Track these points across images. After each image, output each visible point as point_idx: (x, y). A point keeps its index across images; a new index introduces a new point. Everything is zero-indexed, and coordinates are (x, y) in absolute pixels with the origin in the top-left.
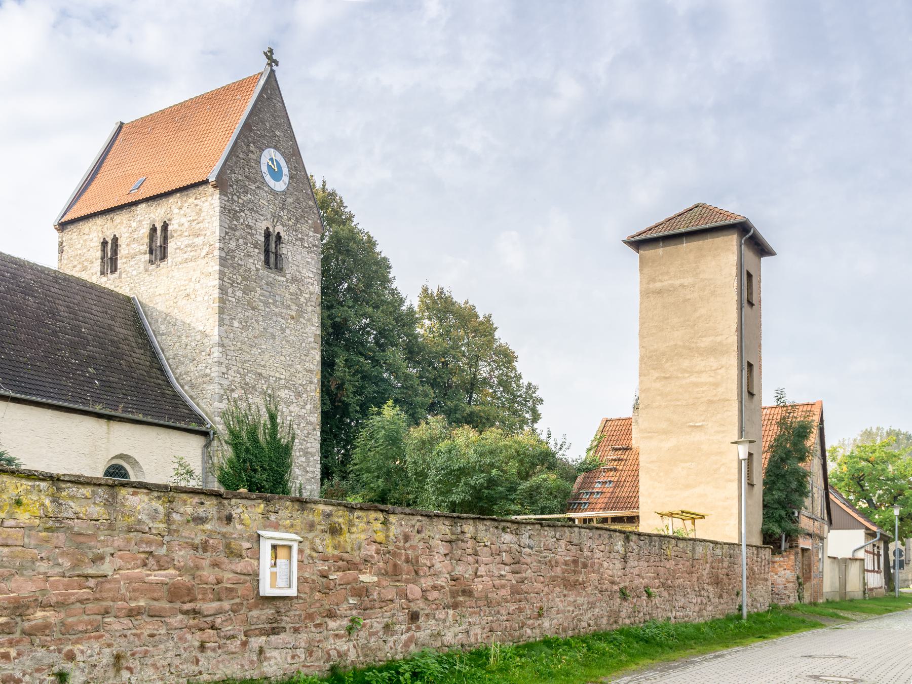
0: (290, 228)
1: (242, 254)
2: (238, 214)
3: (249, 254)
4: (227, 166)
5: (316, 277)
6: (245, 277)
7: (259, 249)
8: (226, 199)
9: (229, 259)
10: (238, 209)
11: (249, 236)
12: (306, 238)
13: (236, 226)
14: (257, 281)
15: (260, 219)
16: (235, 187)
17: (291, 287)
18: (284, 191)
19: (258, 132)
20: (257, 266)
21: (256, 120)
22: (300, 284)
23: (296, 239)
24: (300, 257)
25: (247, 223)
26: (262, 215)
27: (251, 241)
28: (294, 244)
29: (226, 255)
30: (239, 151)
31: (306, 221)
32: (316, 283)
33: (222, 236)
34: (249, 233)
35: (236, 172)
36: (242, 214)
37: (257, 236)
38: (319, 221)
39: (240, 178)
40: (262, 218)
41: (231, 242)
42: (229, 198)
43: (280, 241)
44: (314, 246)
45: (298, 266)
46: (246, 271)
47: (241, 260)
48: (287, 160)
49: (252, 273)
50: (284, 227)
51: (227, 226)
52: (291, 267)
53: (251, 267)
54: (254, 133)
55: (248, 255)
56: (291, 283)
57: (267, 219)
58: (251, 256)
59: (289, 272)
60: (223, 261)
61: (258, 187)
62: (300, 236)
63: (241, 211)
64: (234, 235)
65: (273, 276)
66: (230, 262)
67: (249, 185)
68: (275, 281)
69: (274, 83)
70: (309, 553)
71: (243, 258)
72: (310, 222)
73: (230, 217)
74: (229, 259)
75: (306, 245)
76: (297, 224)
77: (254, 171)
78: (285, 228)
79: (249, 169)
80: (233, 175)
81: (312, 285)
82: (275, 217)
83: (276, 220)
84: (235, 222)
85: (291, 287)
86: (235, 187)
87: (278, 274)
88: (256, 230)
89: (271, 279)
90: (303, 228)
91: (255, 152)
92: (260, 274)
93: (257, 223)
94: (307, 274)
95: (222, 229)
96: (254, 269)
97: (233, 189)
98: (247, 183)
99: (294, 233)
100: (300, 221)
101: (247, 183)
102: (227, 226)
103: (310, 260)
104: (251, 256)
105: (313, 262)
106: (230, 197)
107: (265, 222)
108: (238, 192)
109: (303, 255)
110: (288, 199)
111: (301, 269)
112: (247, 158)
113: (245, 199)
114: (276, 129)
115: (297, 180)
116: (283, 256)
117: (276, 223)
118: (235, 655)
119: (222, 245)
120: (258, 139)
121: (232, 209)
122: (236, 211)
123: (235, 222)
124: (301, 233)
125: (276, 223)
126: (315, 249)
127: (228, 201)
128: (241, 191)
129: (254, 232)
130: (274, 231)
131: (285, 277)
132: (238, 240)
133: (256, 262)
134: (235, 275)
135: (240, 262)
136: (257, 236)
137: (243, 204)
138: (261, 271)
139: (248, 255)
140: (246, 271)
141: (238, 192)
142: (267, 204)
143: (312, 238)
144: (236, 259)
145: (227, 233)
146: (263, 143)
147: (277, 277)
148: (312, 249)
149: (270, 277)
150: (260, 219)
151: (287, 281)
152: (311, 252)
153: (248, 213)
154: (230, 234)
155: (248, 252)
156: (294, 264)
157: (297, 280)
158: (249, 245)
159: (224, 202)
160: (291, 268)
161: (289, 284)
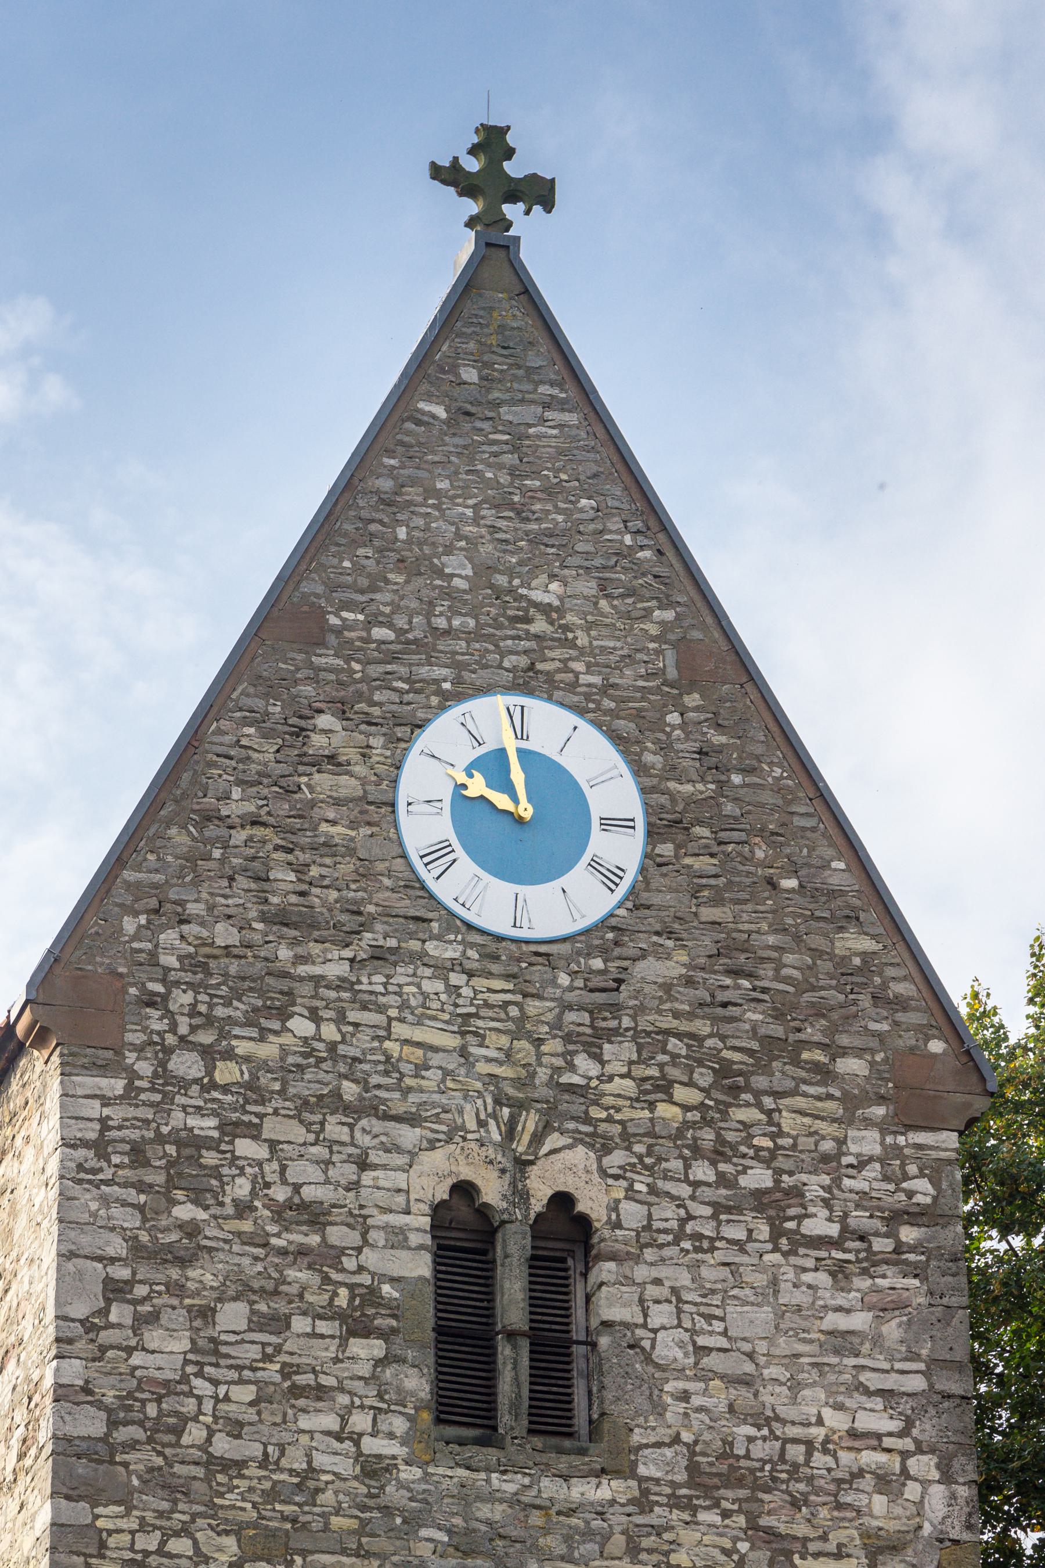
0: (664, 1147)
1: (245, 1394)
2: (210, 1158)
3: (301, 1379)
4: (120, 895)
5: (925, 1429)
6: (273, 1534)
7: (385, 1335)
8: (117, 1086)
9: (132, 1445)
10: (206, 1126)
11: (299, 1275)
12: (815, 1184)
13: (192, 1230)
14: (380, 1544)
15: (393, 1148)
16: (183, 998)
17: (688, 1536)
18: (604, 924)
19: (379, 633)
20: (371, 1445)
21: (358, 568)
22: (773, 1499)
23: (718, 1208)
24: (765, 1314)
25: (280, 1194)
26: (412, 1120)
27: (317, 1299)
28: (704, 1244)
29: (113, 1424)
30: (220, 778)
31: (816, 1067)
32: (923, 1465)
33: (80, 1310)
34: (303, 1251)
35: (193, 908)
36: (245, 1147)
37: (370, 1258)
38: (936, 1046)
39: (225, 934)
40: (409, 1136)
41: (153, 1337)
42: (133, 1075)
43: (588, 1247)
44: (896, 1218)
45: (745, 1381)
46: (273, 1495)
47: (236, 1429)
48: (625, 726)
49: (327, 1497)
50: (606, 1150)
51: (117, 1247)
52: (685, 1396)
53: (321, 1460)
54: (347, 650)
55: (297, 1391)
56: (675, 1502)
57: (455, 1132)
58: (320, 1392)
59: (664, 1434)
60: (82, 1467)
61: (379, 956)
62: (758, 1178)
63: (231, 1130)
64: (176, 1289)
65: (509, 1485)
66: (141, 1459)
67: (301, 959)
68: (536, 1519)
69: (515, 316)
70: (291, 954)
71: (251, 1415)
72: (852, 1066)
73: (141, 1187)
74: (132, 1445)
75: (819, 1225)
76: (724, 1111)
77: (347, 867)
78: (617, 1159)
79: (301, 869)
80: (169, 937)
81: (885, 1483)
82: (519, 1106)
83: (530, 1122)
84: (185, 1212)
85: (688, 1536)
86: (183, 998)
87: (563, 1463)
88: (360, 1222)
89: (497, 1512)
90: (788, 1122)
91: (351, 754)
92: (393, 1494)
93: (367, 1178)
94: (837, 1421)
95: (80, 1273)
96: (346, 1467)
97: (169, 1014)
98: (284, 953)
99: (703, 1171)
100: (760, 1082)
101: (284, 953)
102: (117, 1247)
103: (860, 1321)
104: (320, 1392)
105: (892, 1330)
106: (145, 1068)
107: (436, 1160)
108: (210, 1021)
109: (789, 1296)
110: (650, 970)
111: (774, 1398)
112: (284, 808)
113: (268, 1050)
114: (533, 574)
115: (721, 825)
116: (604, 1341)
117: (537, 1139)
118: (351, 907)
119: (75, 1371)
120: (375, 670)
121: (160, 1139)
122: (197, 1143)
123: (185, 1212)
124: (768, 1158)
125: (537, 1139)
126: (908, 1234)
127: (130, 1094)
128: (238, 1010)
129: (338, 1235)
130: (520, 1195)
131: (631, 1473)
132: (207, 1314)
133: (361, 1421)
134: (184, 1531)
135: (222, 1445)
136: (370, 1258)
137: (251, 1086)
138: (410, 1474)
139: (297, 1391)
140: (273, 1495)
141: (210, 1021)
142: (452, 1041)
143: (873, 1170)
144: (194, 1434)
145: (115, 1290)
146: (417, 686)
147: (550, 1487)
148: (882, 1245)
149: (492, 1497)
150: (393, 1148)
151: (643, 1503)
152: (871, 1263)
153: (297, 1132)
154: (141, 1291)
155: (287, 1372)
156: (705, 1376)
157: (732, 1479)
158: (300, 1324)
159: (94, 1109)
160: (674, 1410)
161: (659, 1515)
